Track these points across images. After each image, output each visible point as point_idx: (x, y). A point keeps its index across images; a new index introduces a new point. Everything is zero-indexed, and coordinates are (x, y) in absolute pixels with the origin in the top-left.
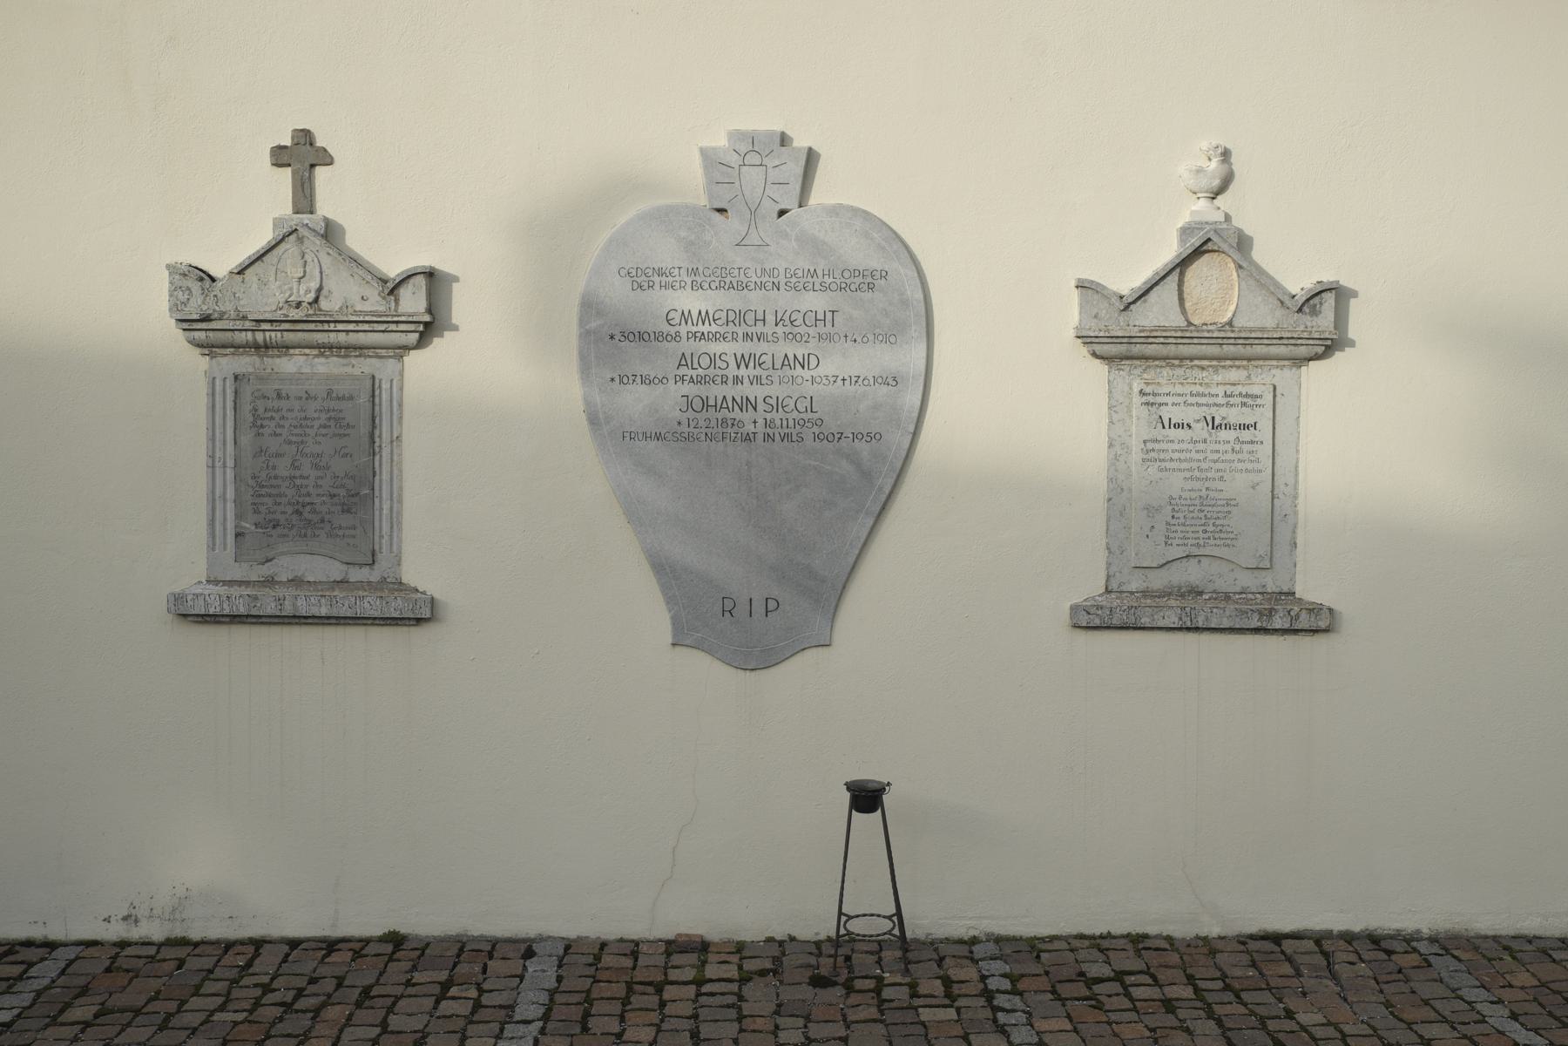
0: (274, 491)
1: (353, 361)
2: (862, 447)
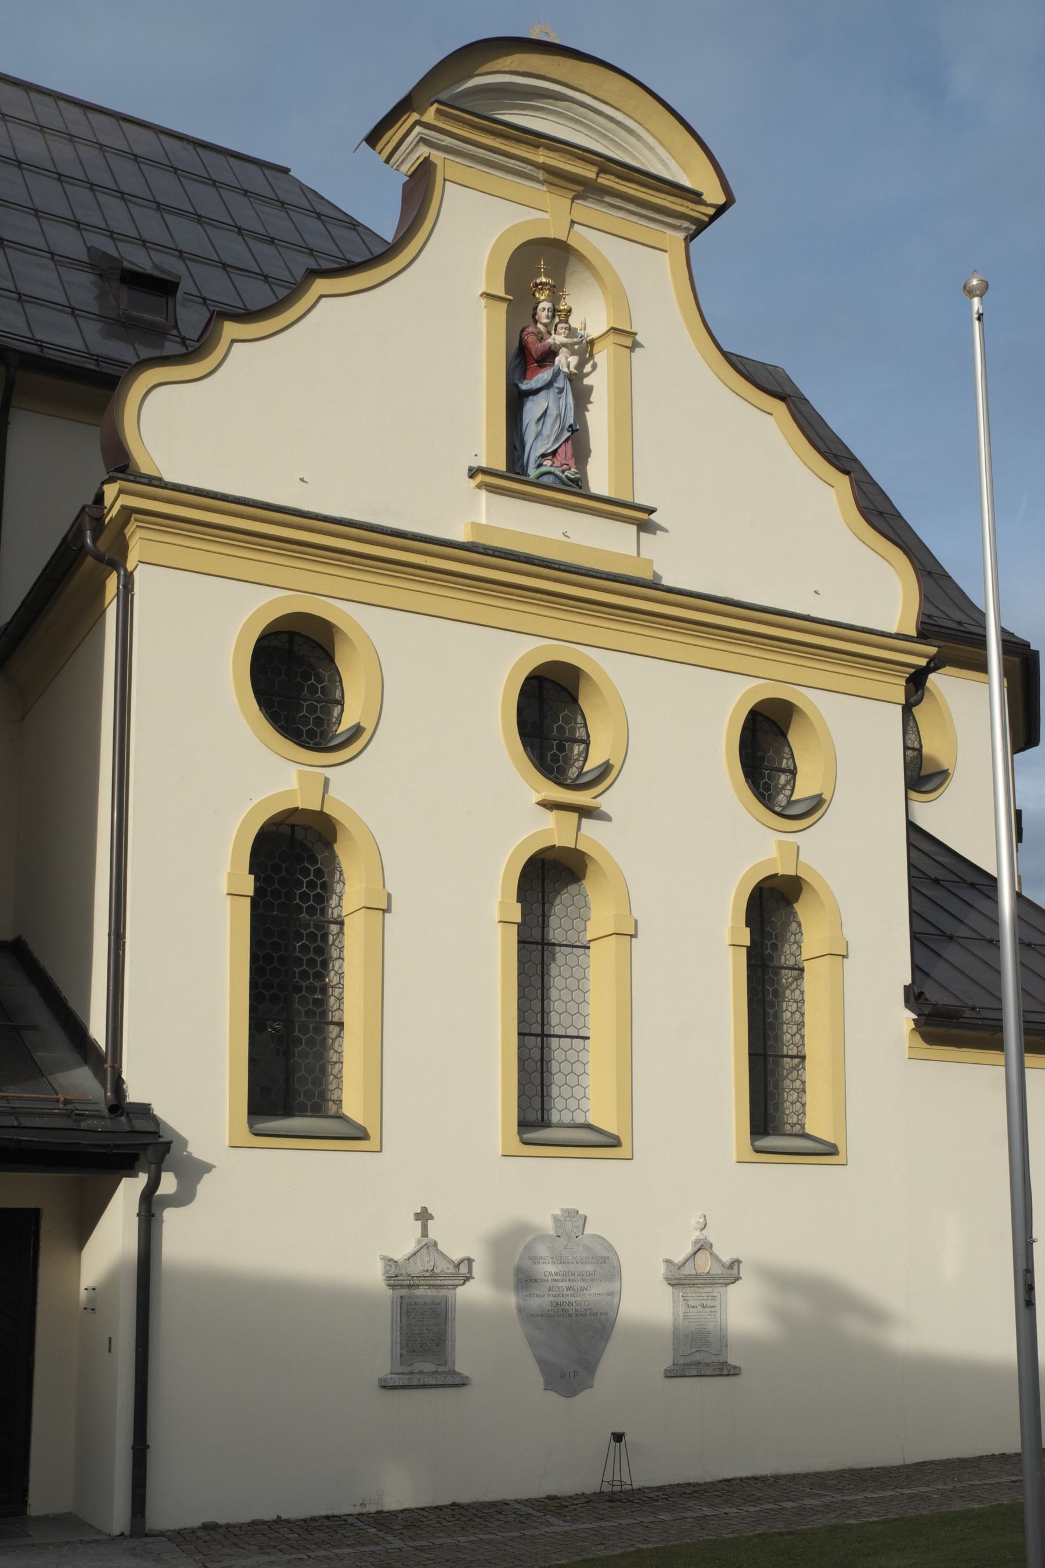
2: (603, 1317)
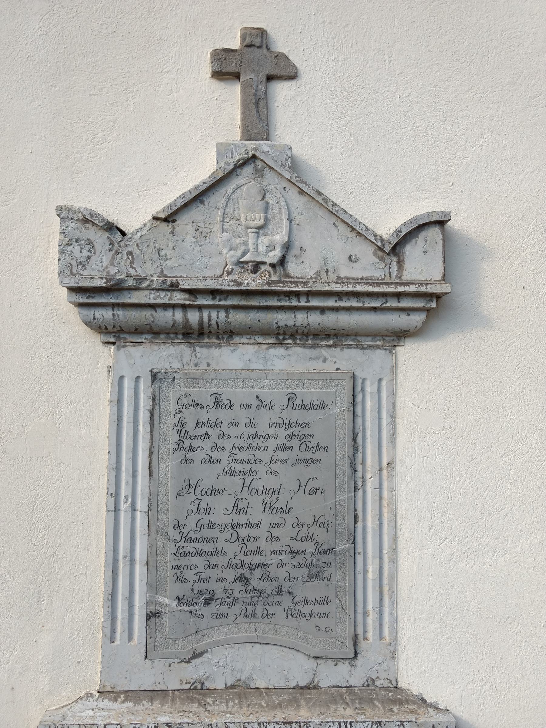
0: (207, 547)
1: (325, 352)
